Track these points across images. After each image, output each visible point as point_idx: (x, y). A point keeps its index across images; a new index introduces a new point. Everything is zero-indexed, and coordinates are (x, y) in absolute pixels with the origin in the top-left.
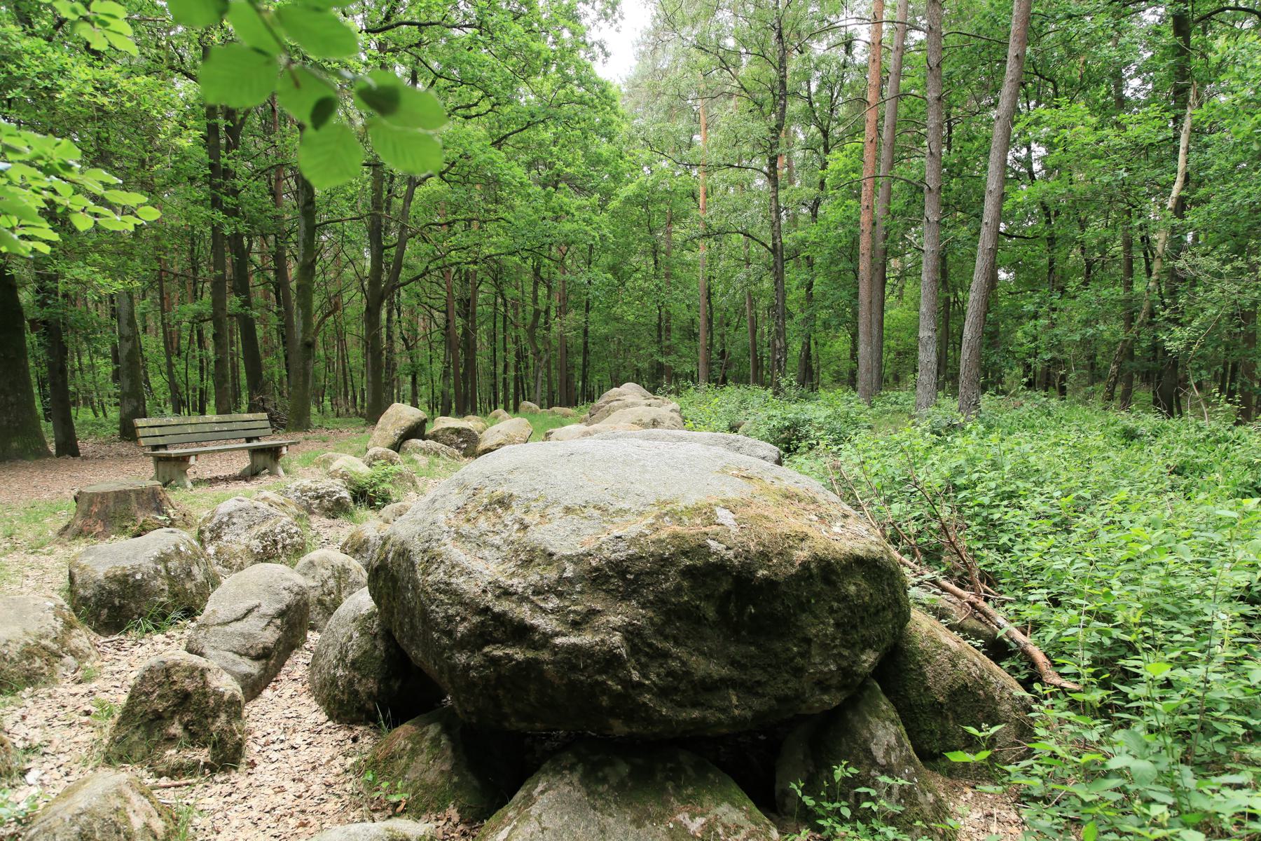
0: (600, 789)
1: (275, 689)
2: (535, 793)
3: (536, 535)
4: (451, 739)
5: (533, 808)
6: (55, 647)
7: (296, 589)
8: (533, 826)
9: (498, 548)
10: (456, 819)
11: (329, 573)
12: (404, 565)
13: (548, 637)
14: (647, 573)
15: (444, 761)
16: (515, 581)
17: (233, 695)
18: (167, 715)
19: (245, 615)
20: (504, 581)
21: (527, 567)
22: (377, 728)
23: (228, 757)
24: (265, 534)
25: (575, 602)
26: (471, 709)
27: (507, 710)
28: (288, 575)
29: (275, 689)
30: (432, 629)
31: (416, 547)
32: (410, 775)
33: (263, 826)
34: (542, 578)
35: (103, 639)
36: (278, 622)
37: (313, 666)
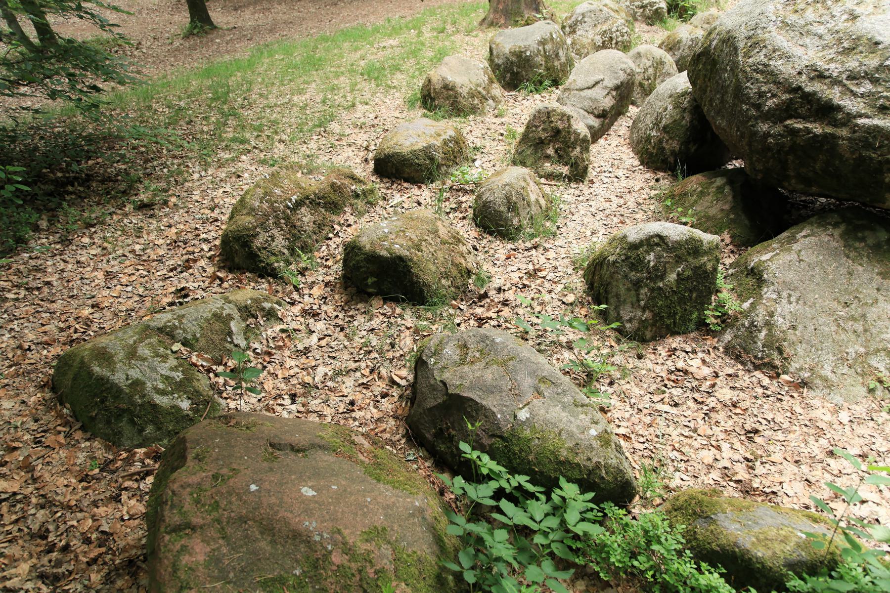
0: (857, 244)
1: (606, 140)
2: (798, 236)
3: (865, 24)
4: (733, 189)
5: (795, 245)
6: (484, 93)
7: (628, 71)
8: (793, 256)
9: (820, 37)
10: (728, 241)
11: (649, 63)
12: (726, 50)
13: (850, 117)
15: (725, 203)
16: (832, 66)
17: (585, 136)
18: (546, 142)
19: (594, 86)
20: (822, 65)
21: (848, 54)
22: (675, 177)
23: (578, 174)
24: (605, 32)
26: (759, 167)
27: (792, 173)
28: (624, 60)
29: (606, 140)
30: (743, 102)
31: (741, 34)
32: (698, 208)
33: (598, 218)
34: (861, 64)
35: (507, 94)
36: (614, 93)
37: (633, 128)
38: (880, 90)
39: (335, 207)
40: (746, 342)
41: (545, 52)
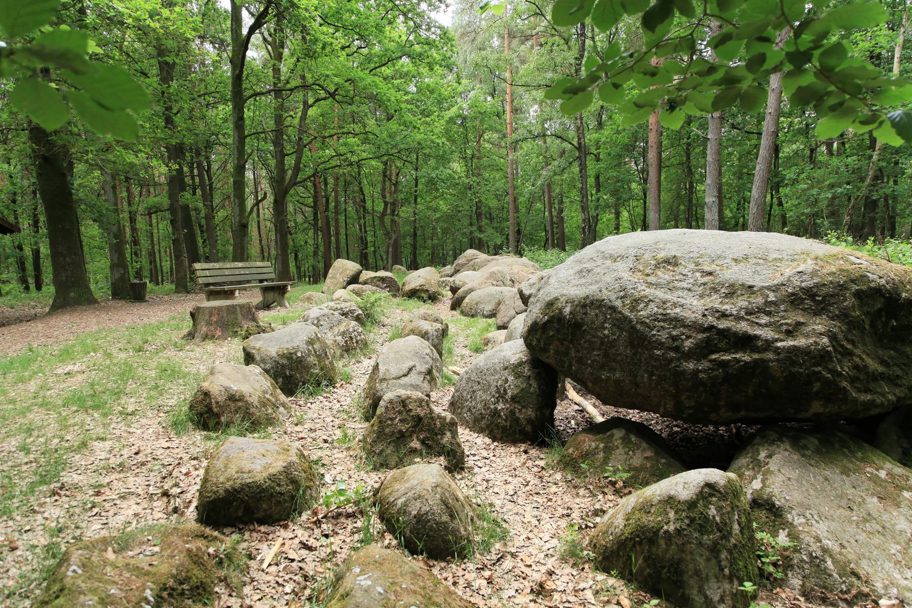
14: (832, 296)
25: (783, 317)
38: (777, 319)
39: (205, 590)
40: (821, 579)
41: (315, 352)
